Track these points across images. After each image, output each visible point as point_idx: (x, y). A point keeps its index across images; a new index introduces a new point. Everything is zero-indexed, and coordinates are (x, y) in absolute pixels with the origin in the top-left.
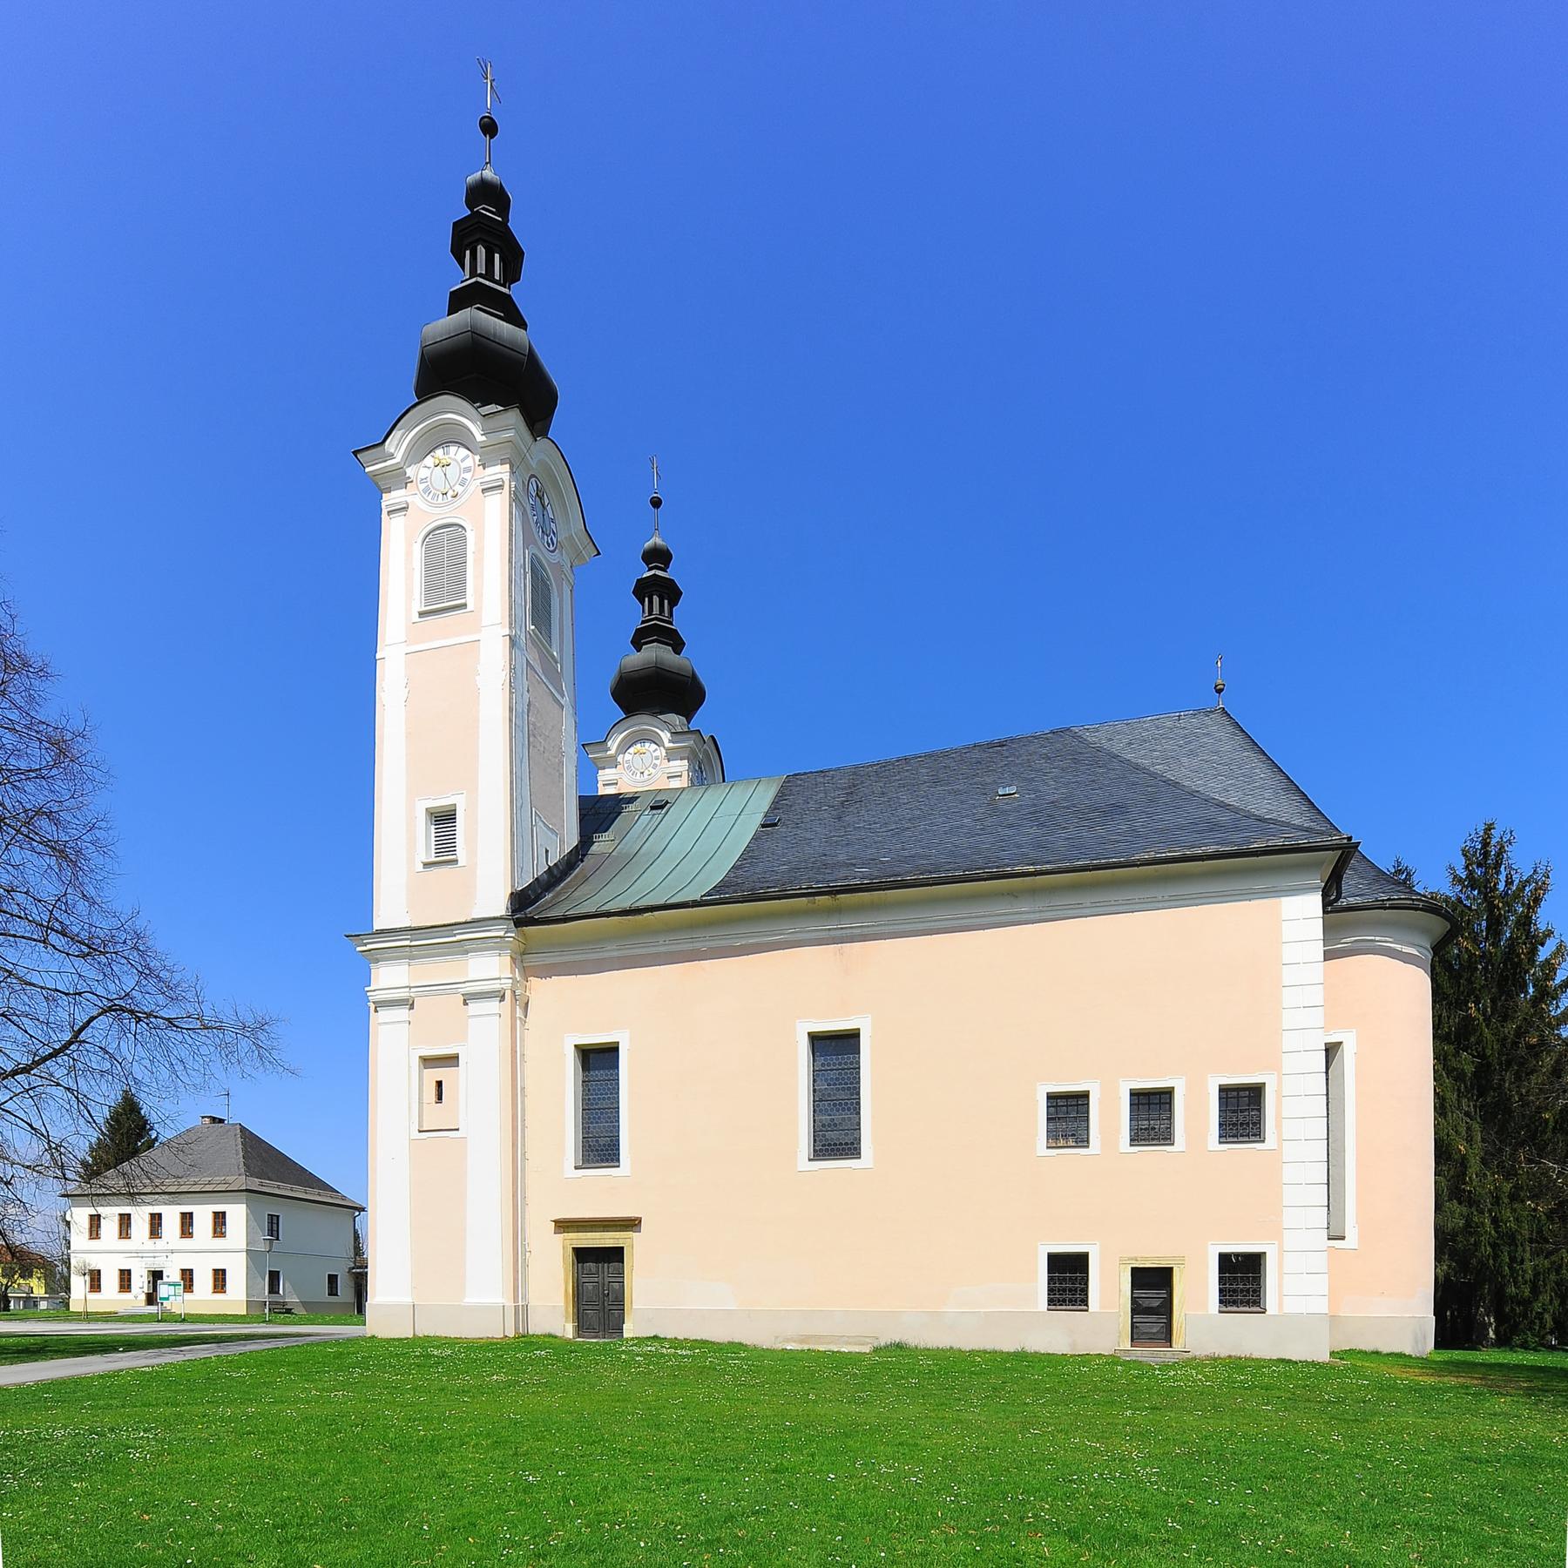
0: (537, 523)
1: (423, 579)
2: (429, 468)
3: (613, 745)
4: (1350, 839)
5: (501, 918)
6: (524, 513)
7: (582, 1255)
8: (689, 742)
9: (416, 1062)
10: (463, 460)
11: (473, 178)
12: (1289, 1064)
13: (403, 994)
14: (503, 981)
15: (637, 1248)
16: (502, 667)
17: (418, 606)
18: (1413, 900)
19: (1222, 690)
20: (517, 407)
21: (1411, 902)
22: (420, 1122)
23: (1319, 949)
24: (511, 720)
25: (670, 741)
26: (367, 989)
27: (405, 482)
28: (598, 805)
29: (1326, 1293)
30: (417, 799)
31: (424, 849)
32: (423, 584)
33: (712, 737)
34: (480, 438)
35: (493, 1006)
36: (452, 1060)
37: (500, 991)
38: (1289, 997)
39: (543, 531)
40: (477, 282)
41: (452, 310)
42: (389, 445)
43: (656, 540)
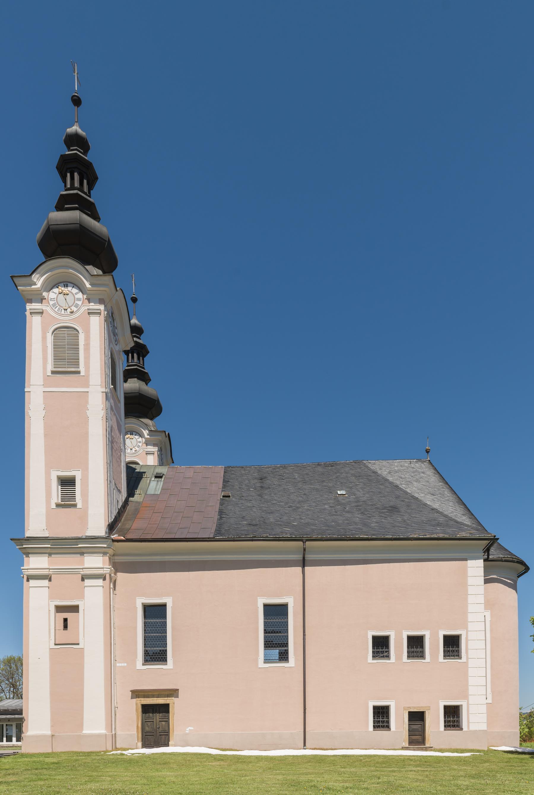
2: (55, 293)
4: (495, 536)
7: (146, 709)
9: (53, 610)
12: (471, 627)
13: (46, 572)
14: (105, 569)
15: (175, 705)
16: (102, 409)
17: (50, 367)
18: (513, 558)
19: (429, 452)
21: (512, 559)
22: (55, 641)
23: (482, 579)
25: (148, 435)
26: (22, 568)
27: (41, 300)
29: (486, 722)
30: (52, 470)
31: (56, 495)
34: (88, 285)
35: (100, 582)
36: (75, 609)
38: (471, 599)
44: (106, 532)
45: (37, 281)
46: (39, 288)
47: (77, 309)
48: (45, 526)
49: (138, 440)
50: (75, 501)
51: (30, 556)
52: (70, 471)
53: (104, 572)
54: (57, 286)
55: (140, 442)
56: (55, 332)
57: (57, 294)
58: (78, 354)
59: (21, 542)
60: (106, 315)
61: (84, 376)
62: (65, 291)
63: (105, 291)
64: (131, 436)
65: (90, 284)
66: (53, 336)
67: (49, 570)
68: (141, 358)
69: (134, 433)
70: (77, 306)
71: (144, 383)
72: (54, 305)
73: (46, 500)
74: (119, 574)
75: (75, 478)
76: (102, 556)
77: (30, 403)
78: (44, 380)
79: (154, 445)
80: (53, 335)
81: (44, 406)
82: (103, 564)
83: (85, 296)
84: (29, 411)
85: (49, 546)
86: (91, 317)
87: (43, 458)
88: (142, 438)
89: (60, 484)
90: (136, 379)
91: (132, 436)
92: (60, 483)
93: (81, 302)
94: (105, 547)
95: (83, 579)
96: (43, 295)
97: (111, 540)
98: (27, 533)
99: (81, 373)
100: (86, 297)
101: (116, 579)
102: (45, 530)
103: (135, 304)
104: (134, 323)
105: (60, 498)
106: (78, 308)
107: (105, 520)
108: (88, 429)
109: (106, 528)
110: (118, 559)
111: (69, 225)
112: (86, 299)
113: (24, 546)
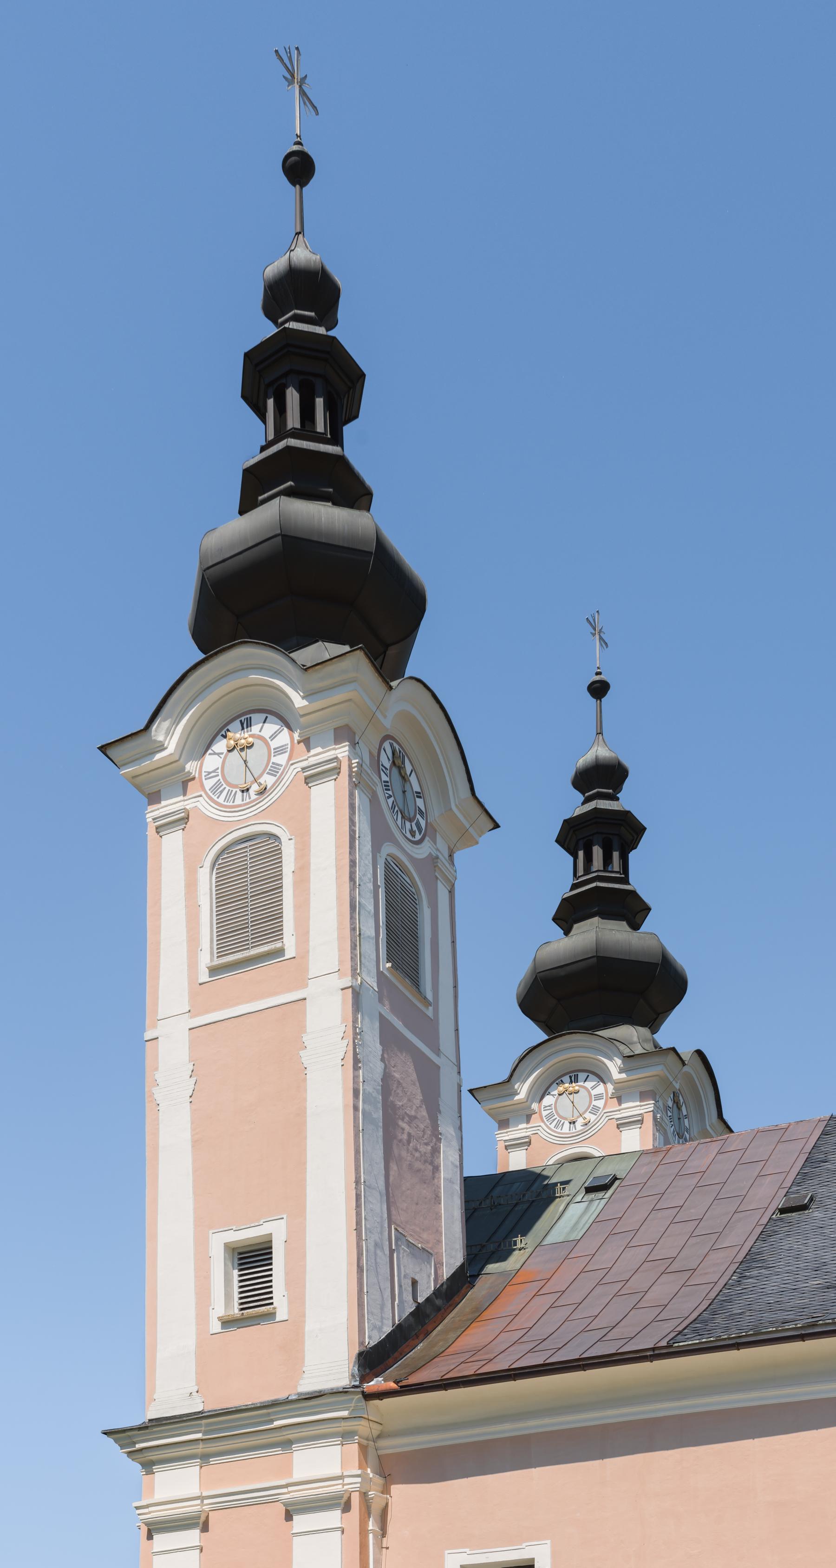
0: (393, 807)
1: (215, 918)
3: (523, 1090)
5: (344, 1392)
6: (374, 801)
8: (655, 1070)
10: (273, 737)
11: (276, 267)
13: (192, 1508)
14: (347, 1480)
16: (342, 1035)
17: (205, 959)
20: (360, 648)
24: (356, 1108)
27: (185, 784)
28: (495, 1193)
30: (211, 1232)
32: (215, 926)
33: (699, 1053)
34: (298, 701)
35: (333, 1518)
37: (341, 1497)
39: (403, 817)
40: (288, 448)
41: (247, 504)
42: (156, 731)
43: (601, 752)
44: (353, 1376)
45: (165, 739)
46: (171, 754)
47: (274, 779)
48: (194, 1383)
49: (594, 1092)
50: (272, 1304)
51: (154, 1471)
52: (257, 1224)
53: (346, 1487)
54: (223, 733)
55: (598, 1097)
56: (220, 861)
57: (556, 1097)
58: (280, 903)
59: (130, 1437)
60: (355, 769)
61: (294, 958)
62: (243, 741)
63: (350, 700)
64: (574, 1084)
65: (303, 698)
66: (215, 872)
67: (202, 1502)
68: (616, 855)
69: (582, 1076)
70: (274, 770)
71: (624, 923)
72: (216, 788)
73: (197, 1315)
74: (397, 1490)
75: (271, 1241)
76: (339, 1442)
77: (157, 1069)
78: (193, 996)
79: (643, 1096)
80: (215, 870)
81: (191, 1067)
82: (343, 1465)
83: (296, 736)
84: (155, 1090)
85: (199, 1436)
86: (312, 788)
87: (188, 1204)
88: (604, 1083)
89: (236, 1265)
90: (596, 920)
91: (575, 1086)
92: (236, 1262)
93: (287, 754)
94: (344, 1419)
95: (289, 1517)
96: (186, 770)
97: (361, 1396)
98: (150, 1409)
99: (286, 952)
100: (299, 736)
101: (387, 1505)
102: (195, 1394)
103: (603, 699)
104: (594, 757)
105: (236, 1301)
106: (278, 775)
107: (350, 1343)
108: (305, 1100)
109: (351, 1365)
110: (391, 1446)
111: (241, 556)
112: (299, 742)
113: (138, 1446)
